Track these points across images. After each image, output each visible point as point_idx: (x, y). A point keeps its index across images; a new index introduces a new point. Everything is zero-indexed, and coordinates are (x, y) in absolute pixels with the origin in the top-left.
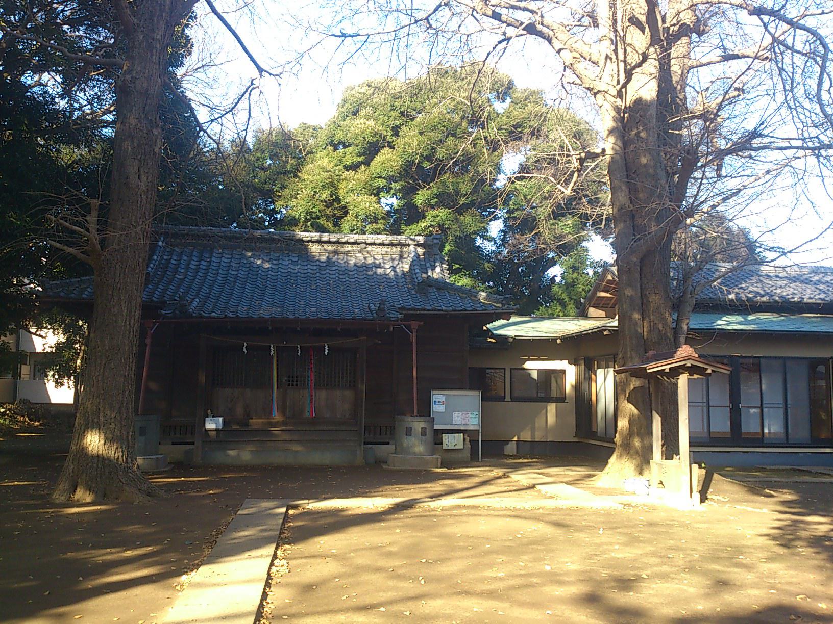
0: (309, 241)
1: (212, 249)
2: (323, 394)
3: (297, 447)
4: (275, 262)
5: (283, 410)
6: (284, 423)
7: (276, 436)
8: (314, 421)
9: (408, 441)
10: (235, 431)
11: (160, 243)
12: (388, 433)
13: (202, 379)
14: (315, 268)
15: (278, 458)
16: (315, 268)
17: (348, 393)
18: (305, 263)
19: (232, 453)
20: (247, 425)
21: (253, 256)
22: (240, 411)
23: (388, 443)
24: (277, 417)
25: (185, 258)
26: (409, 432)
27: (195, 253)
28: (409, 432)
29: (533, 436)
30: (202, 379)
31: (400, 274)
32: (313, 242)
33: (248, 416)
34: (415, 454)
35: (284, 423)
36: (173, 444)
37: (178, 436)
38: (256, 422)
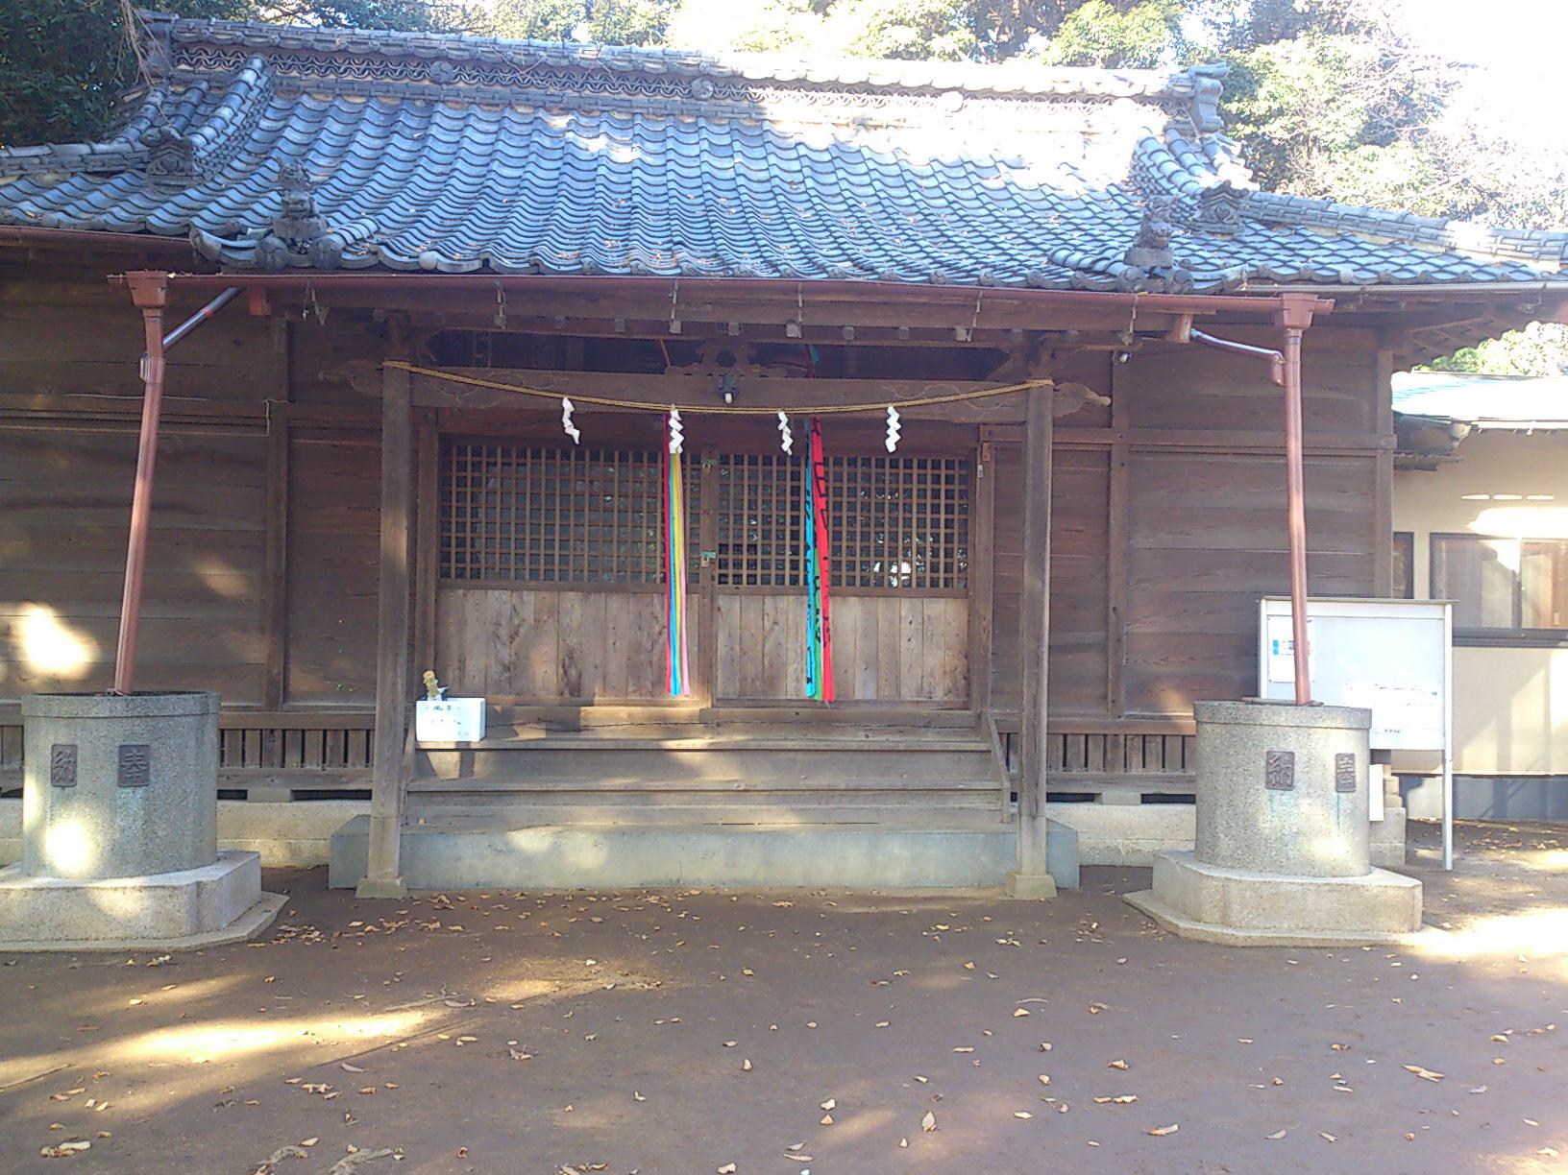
0: (763, 83)
1: (430, 104)
2: (849, 613)
3: (780, 819)
4: (650, 146)
5: (705, 674)
6: (707, 722)
7: (692, 771)
8: (824, 716)
9: (1275, 813)
10: (542, 750)
11: (249, 76)
12: (1095, 756)
13: (396, 539)
14: (795, 166)
15: (702, 865)
16: (795, 166)
17: (945, 613)
18: (759, 153)
19: (530, 841)
20: (574, 727)
21: (574, 127)
22: (544, 672)
23: (1089, 798)
24: (686, 699)
25: (336, 128)
26: (1281, 774)
27: (368, 114)
28: (1281, 774)
29: (1503, 758)
30: (396, 539)
31: (1301, 34)
32: (780, 85)
33: (575, 691)
34: (1310, 867)
35: (707, 722)
36: (300, 796)
37: (313, 766)
38: (610, 717)
